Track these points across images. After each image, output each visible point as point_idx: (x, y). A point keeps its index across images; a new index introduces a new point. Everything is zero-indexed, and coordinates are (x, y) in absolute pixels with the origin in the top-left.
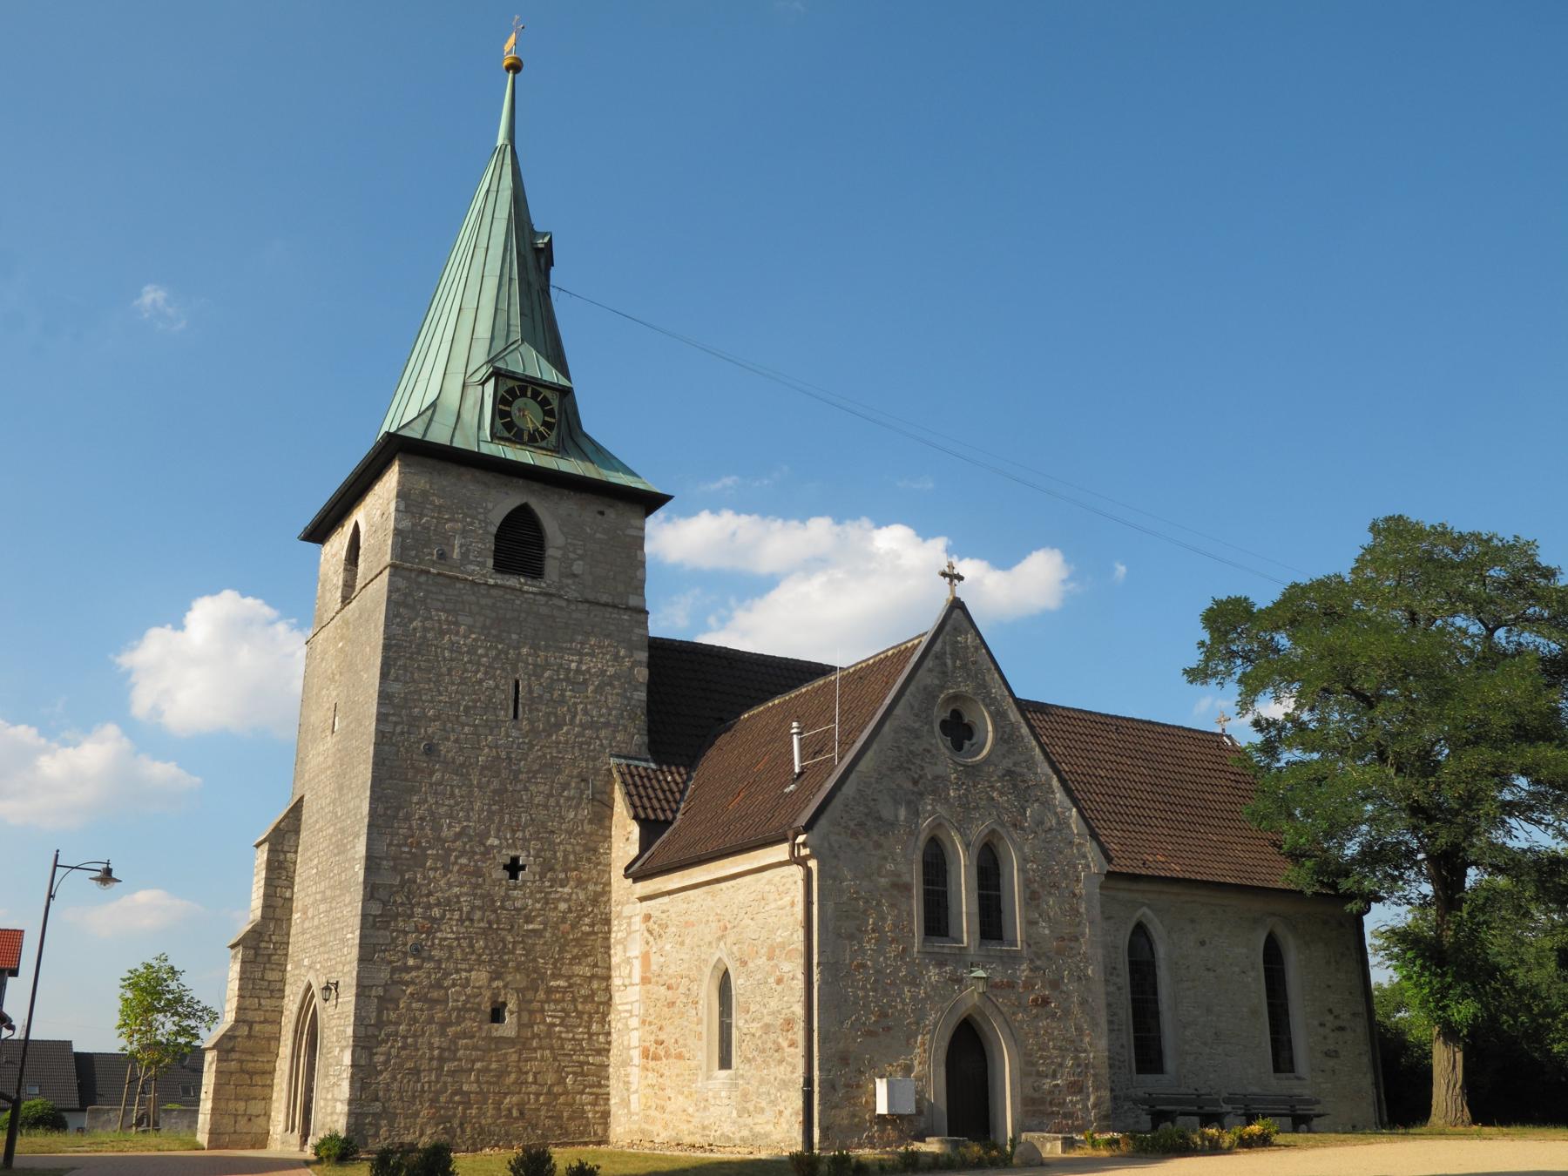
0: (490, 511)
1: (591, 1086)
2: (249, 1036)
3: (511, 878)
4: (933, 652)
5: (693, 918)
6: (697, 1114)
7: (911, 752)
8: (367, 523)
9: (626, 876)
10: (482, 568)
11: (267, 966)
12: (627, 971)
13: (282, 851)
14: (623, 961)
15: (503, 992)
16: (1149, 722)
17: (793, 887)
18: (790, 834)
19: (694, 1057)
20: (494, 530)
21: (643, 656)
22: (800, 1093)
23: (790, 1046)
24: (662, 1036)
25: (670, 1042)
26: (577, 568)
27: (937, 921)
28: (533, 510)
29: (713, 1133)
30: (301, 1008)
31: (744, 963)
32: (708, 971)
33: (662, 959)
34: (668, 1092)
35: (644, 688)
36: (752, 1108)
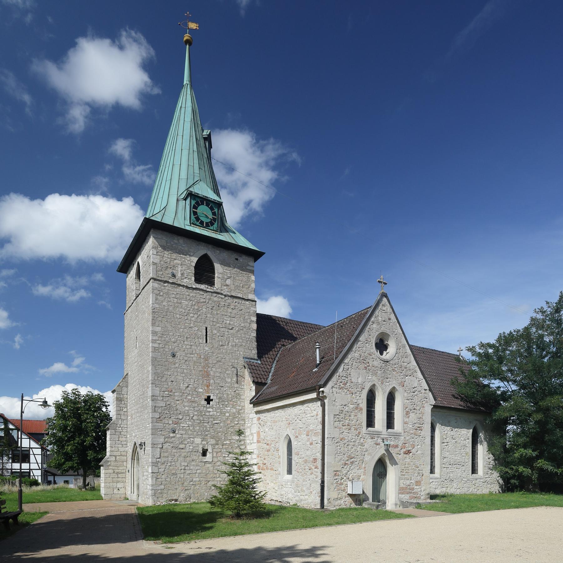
2: (116, 460)
3: (207, 404)
5: (276, 419)
6: (279, 490)
8: (142, 261)
9: (251, 403)
10: (190, 281)
12: (252, 438)
13: (122, 394)
14: (250, 434)
15: (206, 446)
16: (435, 350)
17: (318, 408)
18: (317, 387)
19: (278, 470)
21: (254, 319)
22: (319, 485)
23: (316, 468)
24: (265, 462)
25: (268, 464)
26: (228, 282)
28: (209, 257)
29: (285, 497)
30: (133, 451)
31: (297, 437)
32: (282, 439)
33: (265, 434)
34: (268, 481)
35: (255, 332)
36: (300, 490)
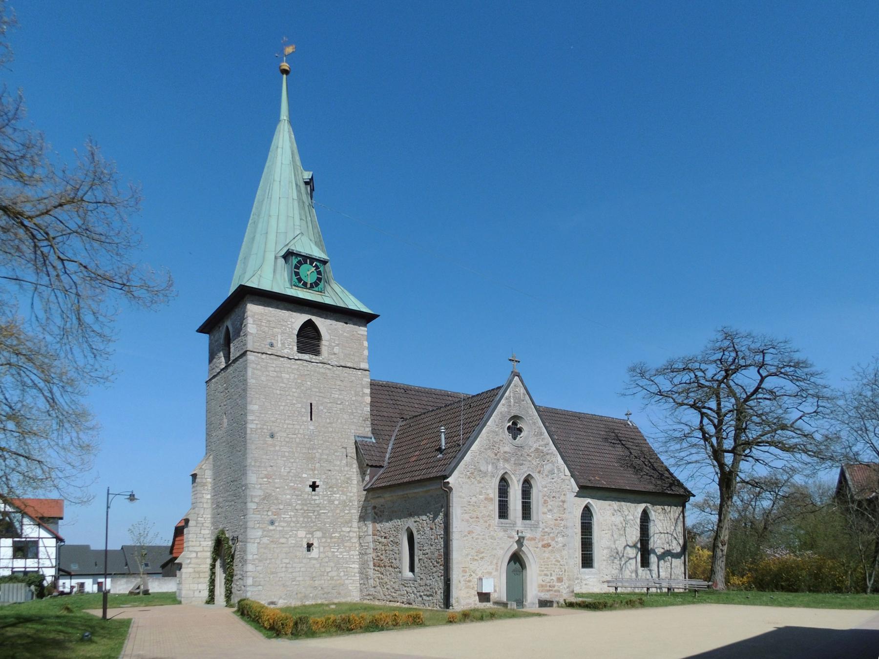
0: (293, 323)
1: (352, 576)
2: (197, 557)
4: (505, 396)
7: (494, 442)
8: (233, 328)
11: (202, 528)
20: (296, 332)
26: (336, 350)
27: (503, 512)
